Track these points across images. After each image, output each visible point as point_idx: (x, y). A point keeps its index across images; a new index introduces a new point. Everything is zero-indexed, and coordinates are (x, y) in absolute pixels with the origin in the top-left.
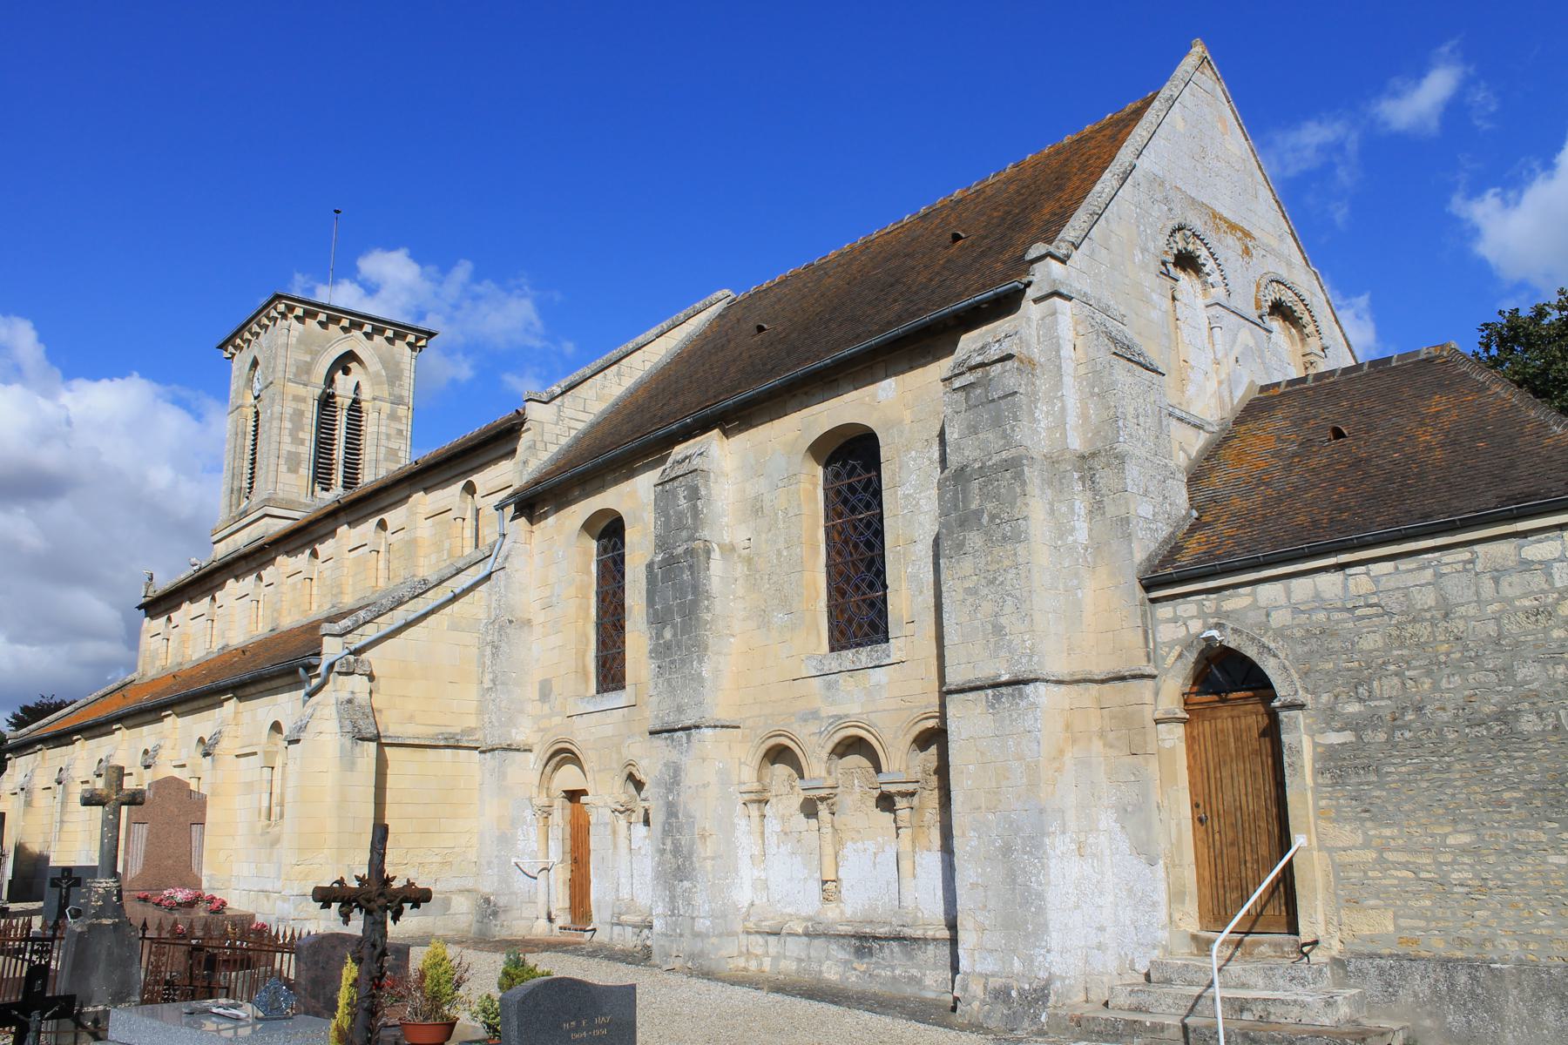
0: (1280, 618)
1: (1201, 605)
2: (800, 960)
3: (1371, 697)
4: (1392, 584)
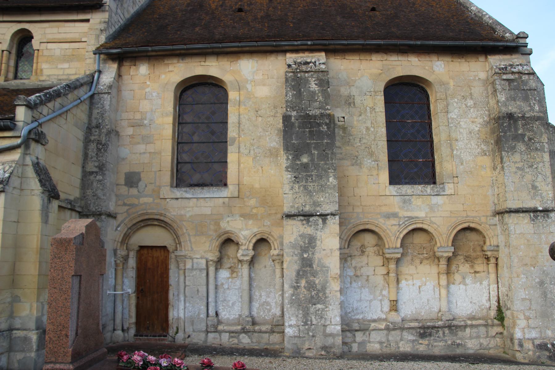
2: (381, 343)
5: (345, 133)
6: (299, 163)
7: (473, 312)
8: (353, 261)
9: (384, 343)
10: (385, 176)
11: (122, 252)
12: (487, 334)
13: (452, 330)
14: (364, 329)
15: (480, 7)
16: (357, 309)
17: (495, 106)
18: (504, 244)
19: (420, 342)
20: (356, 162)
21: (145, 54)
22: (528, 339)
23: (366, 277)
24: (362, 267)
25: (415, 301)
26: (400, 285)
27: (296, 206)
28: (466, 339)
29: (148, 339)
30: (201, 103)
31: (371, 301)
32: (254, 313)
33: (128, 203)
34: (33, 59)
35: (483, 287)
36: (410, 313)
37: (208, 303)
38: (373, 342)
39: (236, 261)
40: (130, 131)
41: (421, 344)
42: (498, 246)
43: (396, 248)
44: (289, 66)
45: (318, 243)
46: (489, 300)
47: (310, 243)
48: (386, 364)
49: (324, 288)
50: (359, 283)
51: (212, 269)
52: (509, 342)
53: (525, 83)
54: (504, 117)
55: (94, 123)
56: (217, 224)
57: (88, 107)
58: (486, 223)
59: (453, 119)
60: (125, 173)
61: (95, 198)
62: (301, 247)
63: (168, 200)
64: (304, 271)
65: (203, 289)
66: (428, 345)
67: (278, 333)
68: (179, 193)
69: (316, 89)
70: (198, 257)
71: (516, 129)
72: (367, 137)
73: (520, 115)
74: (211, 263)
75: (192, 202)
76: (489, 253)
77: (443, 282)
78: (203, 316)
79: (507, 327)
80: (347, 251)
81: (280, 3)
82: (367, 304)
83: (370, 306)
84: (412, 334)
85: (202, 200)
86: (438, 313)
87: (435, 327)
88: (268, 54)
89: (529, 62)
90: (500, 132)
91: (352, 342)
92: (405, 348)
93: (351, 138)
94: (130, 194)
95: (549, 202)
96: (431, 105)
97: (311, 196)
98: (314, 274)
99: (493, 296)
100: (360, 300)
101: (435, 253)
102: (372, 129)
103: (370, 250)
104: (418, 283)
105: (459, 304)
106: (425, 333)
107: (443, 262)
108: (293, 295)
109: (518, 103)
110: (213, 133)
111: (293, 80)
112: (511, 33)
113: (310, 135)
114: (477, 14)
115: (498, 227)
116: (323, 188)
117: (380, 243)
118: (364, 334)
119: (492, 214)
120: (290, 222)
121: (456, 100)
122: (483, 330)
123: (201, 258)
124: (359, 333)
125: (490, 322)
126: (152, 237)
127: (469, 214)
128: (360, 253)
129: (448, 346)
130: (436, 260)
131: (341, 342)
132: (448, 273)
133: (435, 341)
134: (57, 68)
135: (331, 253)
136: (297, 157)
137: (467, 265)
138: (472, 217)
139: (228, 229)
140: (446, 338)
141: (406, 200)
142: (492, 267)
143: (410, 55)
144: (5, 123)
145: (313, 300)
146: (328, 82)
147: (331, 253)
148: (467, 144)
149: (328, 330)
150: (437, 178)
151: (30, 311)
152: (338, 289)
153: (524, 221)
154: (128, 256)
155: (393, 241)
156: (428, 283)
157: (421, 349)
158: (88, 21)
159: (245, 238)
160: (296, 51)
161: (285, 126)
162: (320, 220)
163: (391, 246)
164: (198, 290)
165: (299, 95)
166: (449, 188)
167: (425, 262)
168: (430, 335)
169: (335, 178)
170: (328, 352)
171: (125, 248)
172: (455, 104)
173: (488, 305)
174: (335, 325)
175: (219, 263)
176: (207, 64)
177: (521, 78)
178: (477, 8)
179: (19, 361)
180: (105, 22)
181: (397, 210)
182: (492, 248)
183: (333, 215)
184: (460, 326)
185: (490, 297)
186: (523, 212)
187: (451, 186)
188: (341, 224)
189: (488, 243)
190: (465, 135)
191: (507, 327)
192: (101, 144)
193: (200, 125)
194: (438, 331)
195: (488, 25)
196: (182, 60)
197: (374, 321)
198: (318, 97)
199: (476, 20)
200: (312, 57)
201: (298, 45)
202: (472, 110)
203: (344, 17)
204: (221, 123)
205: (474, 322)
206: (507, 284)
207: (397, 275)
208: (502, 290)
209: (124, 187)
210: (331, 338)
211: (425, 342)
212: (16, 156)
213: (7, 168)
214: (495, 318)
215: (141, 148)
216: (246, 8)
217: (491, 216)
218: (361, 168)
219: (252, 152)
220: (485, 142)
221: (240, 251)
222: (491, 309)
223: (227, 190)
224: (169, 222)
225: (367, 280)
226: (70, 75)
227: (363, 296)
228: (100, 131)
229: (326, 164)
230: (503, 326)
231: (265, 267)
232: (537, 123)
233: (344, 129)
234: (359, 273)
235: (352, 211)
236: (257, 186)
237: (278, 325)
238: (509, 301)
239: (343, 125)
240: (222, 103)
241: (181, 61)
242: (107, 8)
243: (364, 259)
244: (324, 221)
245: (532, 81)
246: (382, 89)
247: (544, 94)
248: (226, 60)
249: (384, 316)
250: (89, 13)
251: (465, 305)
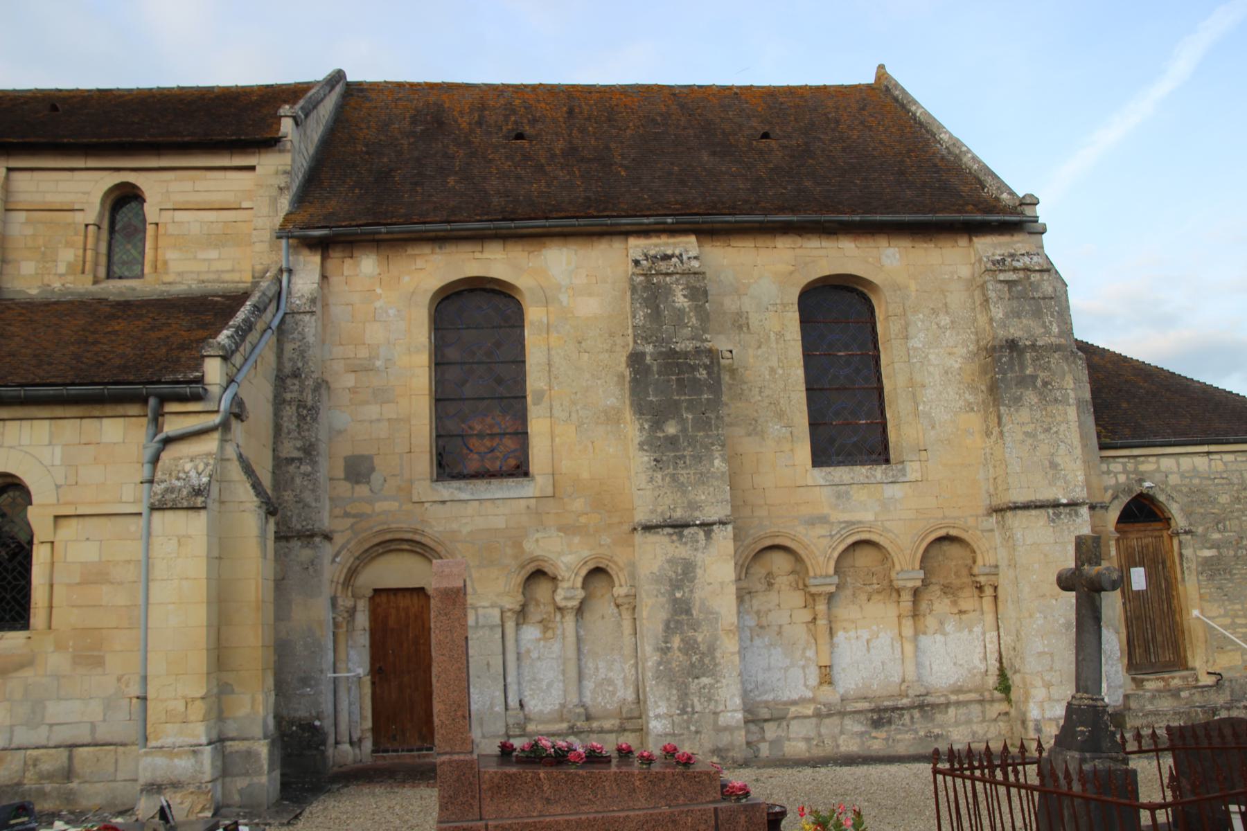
0: (1174, 479)
1: (1124, 465)
2: (808, 740)
3: (1225, 530)
4: (1234, 468)
5: (734, 379)
6: (661, 435)
7: (958, 680)
10: (804, 452)
11: (345, 602)
12: (984, 717)
14: (779, 718)
15: (956, 135)
17: (988, 328)
19: (873, 734)
20: (755, 428)
21: (371, 237)
22: (1050, 719)
23: (776, 628)
25: (861, 666)
26: (835, 639)
27: (659, 510)
29: (399, 757)
30: (477, 328)
31: (786, 669)
32: (587, 700)
33: (353, 512)
34: (143, 240)
37: (505, 686)
39: (551, 609)
40: (349, 380)
41: (875, 738)
42: (996, 566)
43: (827, 576)
44: (637, 263)
45: (699, 572)
47: (685, 573)
48: (823, 770)
49: (712, 649)
51: (510, 625)
52: (1019, 726)
53: (1035, 287)
54: (1002, 347)
55: (288, 367)
56: (518, 545)
57: (275, 339)
59: (915, 349)
60: (345, 458)
61: (300, 505)
62: (671, 580)
63: (427, 505)
64: (678, 622)
65: (497, 661)
66: (887, 739)
67: (633, 731)
68: (448, 490)
69: (686, 305)
70: (486, 604)
71: (1023, 367)
72: (772, 386)
73: (1028, 343)
74: (509, 614)
75: (471, 508)
76: (982, 579)
77: (908, 630)
78: (499, 708)
79: (1016, 703)
80: (744, 584)
81: (589, 119)
83: (786, 678)
85: (488, 504)
87: (898, 709)
88: (595, 238)
89: (1042, 247)
90: (996, 373)
91: (759, 741)
92: (849, 746)
93: (745, 387)
94: (356, 495)
95: (1077, 490)
96: (878, 325)
97: (684, 492)
98: (695, 626)
100: (769, 669)
101: (891, 581)
102: (780, 371)
103: (783, 581)
104: (865, 635)
105: (935, 667)
106: (880, 719)
107: (907, 597)
108: (659, 664)
109: (1025, 321)
110: (499, 381)
111: (645, 289)
112: (1012, 193)
113: (677, 385)
114: (951, 148)
115: (997, 533)
116: (703, 479)
117: (798, 568)
118: (779, 726)
120: (651, 538)
121: (921, 316)
122: (976, 709)
123: (492, 606)
126: (397, 572)
128: (765, 586)
129: (920, 739)
130: (894, 595)
131: (744, 741)
132: (915, 615)
133: (898, 731)
134: (195, 258)
136: (657, 425)
137: (947, 601)
139: (538, 552)
141: (841, 493)
142: (987, 602)
143: (841, 238)
144: (194, 390)
145: (695, 671)
146: (706, 293)
148: (941, 393)
149: (722, 720)
150: (891, 452)
151: (252, 707)
152: (736, 649)
153: (1038, 520)
154: (354, 609)
156: (881, 635)
157: (875, 747)
158: (252, 168)
159: (568, 568)
160: (645, 233)
161: (636, 372)
162: (702, 534)
163: (818, 573)
164: (488, 664)
165: (656, 315)
166: (913, 470)
167: (876, 597)
168: (890, 722)
169: (723, 460)
170: (723, 758)
171: (350, 594)
172: (919, 324)
173: (982, 667)
175: (522, 614)
176: (486, 255)
177: (1029, 278)
178: (951, 137)
179: (240, 792)
180: (285, 172)
181: (826, 511)
182: (987, 570)
183: (722, 523)
184: (938, 705)
186: (1036, 507)
187: (916, 465)
188: (736, 538)
189: (980, 561)
190: (937, 377)
191: (1016, 703)
192: (305, 407)
193: (475, 366)
195: (970, 173)
196: (440, 248)
197: (794, 703)
198: (690, 318)
199: (948, 161)
200: (675, 245)
201: (649, 224)
202: (947, 334)
203: (714, 153)
204: (513, 362)
205: (961, 697)
209: (343, 483)
210: (727, 733)
211: (881, 734)
212: (211, 444)
213: (201, 467)
215: (373, 411)
216: (527, 129)
218: (763, 439)
219: (574, 415)
220: (972, 388)
221: (559, 591)
223: (532, 484)
224: (432, 544)
225: (779, 633)
226: (223, 272)
228: (302, 382)
229: (708, 436)
230: (1009, 701)
231: (603, 617)
232: (1056, 355)
233: (733, 371)
234: (764, 622)
236: (585, 475)
237: (631, 718)
239: (731, 365)
240: (513, 326)
241: (437, 250)
242: (289, 146)
243: (773, 597)
244: (708, 535)
245: (1046, 284)
246: (796, 300)
247: (1067, 301)
248: (520, 248)
249: (810, 694)
250: (254, 153)
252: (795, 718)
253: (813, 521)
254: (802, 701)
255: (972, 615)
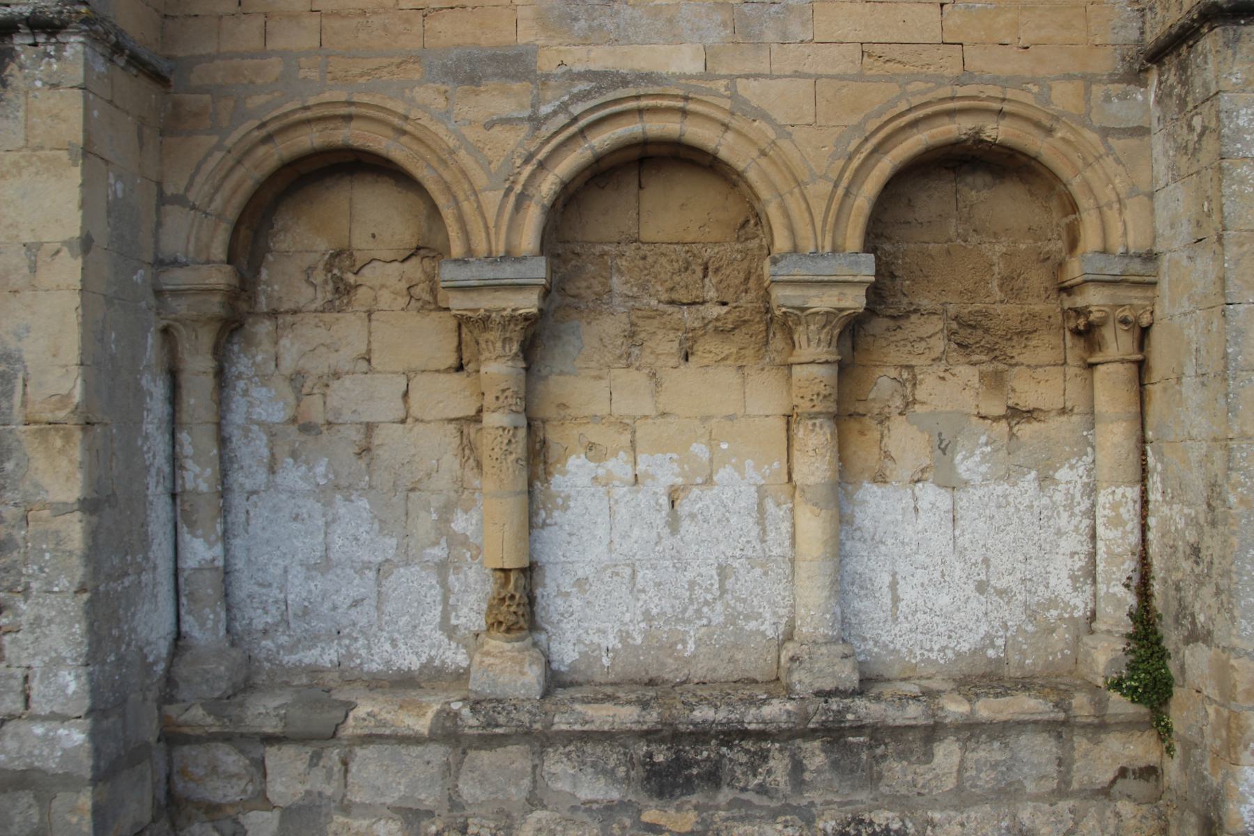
7: (989, 640)
8: (285, 342)
9: (430, 814)
12: (1065, 781)
13: (849, 748)
16: (306, 612)
18: (1186, 230)
19: (650, 816)
23: (355, 435)
24: (337, 375)
25: (645, 575)
28: (934, 803)
35: (1059, 497)
36: (612, 641)
38: (367, 809)
46: (1090, 573)
50: (320, 469)
58: (1084, 120)
76: (1094, 299)
77: (814, 466)
82: (361, 586)
83: (381, 597)
84: (601, 770)
86: (780, 646)
87: (745, 734)
91: (246, 805)
99: (1110, 553)
100: (325, 564)
103: (384, 280)
104: (664, 471)
105: (908, 594)
106: (679, 764)
115: (1158, 143)
118: (315, 759)
119: (1120, 68)
122: (1037, 752)
124: (289, 751)
125: (1081, 704)
127: (977, 61)
132: (846, 412)
135: (33, 268)
137: (967, 373)
138: (995, 81)
140: (809, 796)
142: (1111, 386)
147: (33, 268)
155: (491, 214)
156: (723, 474)
167: (710, 347)
168: (713, 778)
173: (1079, 603)
174: (53, 717)
181: (527, 35)
182: (1115, 268)
184: (898, 732)
185: (1093, 555)
189: (1090, 239)
191: (1189, 746)
194: (764, 756)
206: (1197, 481)
207: (532, 425)
208: (1165, 521)
210: (26, 798)
214: (1117, 685)
217: (1113, 79)
222: (1099, 625)
225: (365, 450)
227: (338, 542)
234: (315, 411)
235: (257, 43)
238: (1207, 591)
243: (349, 330)
249: (456, 657)
251: (944, 600)
252: (368, 739)
253: (469, 71)
254: (402, 683)
255: (1056, 427)
